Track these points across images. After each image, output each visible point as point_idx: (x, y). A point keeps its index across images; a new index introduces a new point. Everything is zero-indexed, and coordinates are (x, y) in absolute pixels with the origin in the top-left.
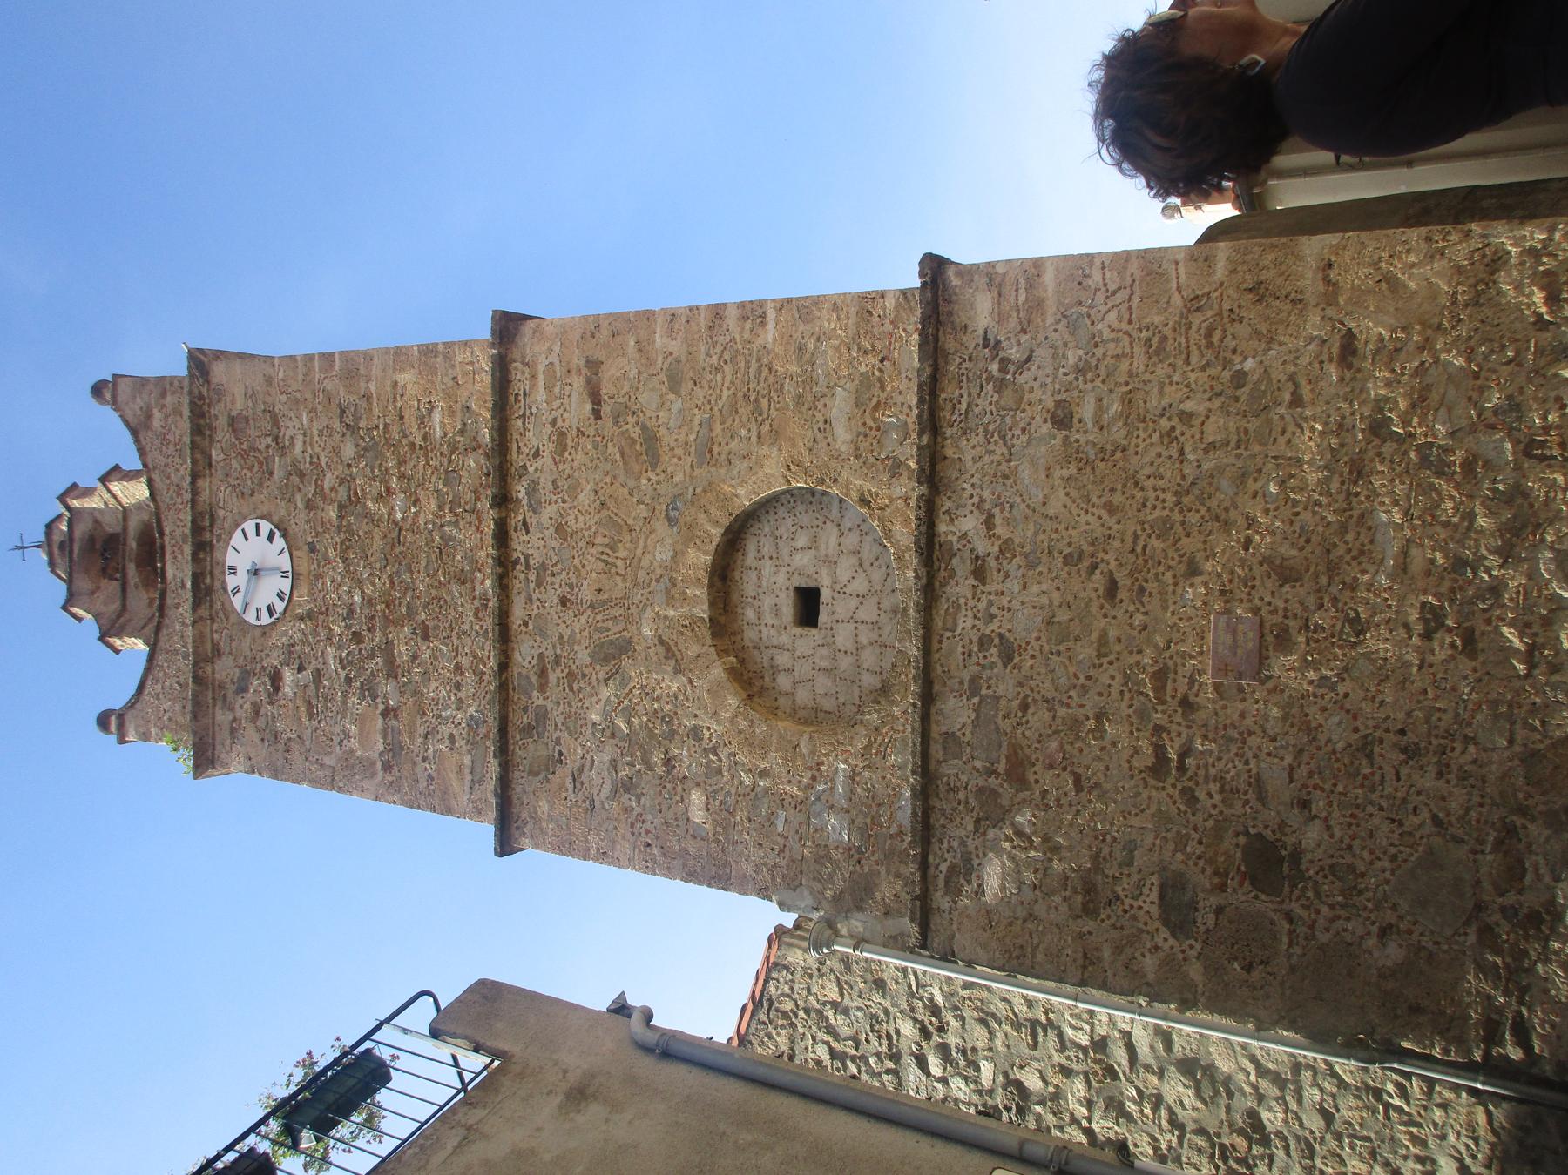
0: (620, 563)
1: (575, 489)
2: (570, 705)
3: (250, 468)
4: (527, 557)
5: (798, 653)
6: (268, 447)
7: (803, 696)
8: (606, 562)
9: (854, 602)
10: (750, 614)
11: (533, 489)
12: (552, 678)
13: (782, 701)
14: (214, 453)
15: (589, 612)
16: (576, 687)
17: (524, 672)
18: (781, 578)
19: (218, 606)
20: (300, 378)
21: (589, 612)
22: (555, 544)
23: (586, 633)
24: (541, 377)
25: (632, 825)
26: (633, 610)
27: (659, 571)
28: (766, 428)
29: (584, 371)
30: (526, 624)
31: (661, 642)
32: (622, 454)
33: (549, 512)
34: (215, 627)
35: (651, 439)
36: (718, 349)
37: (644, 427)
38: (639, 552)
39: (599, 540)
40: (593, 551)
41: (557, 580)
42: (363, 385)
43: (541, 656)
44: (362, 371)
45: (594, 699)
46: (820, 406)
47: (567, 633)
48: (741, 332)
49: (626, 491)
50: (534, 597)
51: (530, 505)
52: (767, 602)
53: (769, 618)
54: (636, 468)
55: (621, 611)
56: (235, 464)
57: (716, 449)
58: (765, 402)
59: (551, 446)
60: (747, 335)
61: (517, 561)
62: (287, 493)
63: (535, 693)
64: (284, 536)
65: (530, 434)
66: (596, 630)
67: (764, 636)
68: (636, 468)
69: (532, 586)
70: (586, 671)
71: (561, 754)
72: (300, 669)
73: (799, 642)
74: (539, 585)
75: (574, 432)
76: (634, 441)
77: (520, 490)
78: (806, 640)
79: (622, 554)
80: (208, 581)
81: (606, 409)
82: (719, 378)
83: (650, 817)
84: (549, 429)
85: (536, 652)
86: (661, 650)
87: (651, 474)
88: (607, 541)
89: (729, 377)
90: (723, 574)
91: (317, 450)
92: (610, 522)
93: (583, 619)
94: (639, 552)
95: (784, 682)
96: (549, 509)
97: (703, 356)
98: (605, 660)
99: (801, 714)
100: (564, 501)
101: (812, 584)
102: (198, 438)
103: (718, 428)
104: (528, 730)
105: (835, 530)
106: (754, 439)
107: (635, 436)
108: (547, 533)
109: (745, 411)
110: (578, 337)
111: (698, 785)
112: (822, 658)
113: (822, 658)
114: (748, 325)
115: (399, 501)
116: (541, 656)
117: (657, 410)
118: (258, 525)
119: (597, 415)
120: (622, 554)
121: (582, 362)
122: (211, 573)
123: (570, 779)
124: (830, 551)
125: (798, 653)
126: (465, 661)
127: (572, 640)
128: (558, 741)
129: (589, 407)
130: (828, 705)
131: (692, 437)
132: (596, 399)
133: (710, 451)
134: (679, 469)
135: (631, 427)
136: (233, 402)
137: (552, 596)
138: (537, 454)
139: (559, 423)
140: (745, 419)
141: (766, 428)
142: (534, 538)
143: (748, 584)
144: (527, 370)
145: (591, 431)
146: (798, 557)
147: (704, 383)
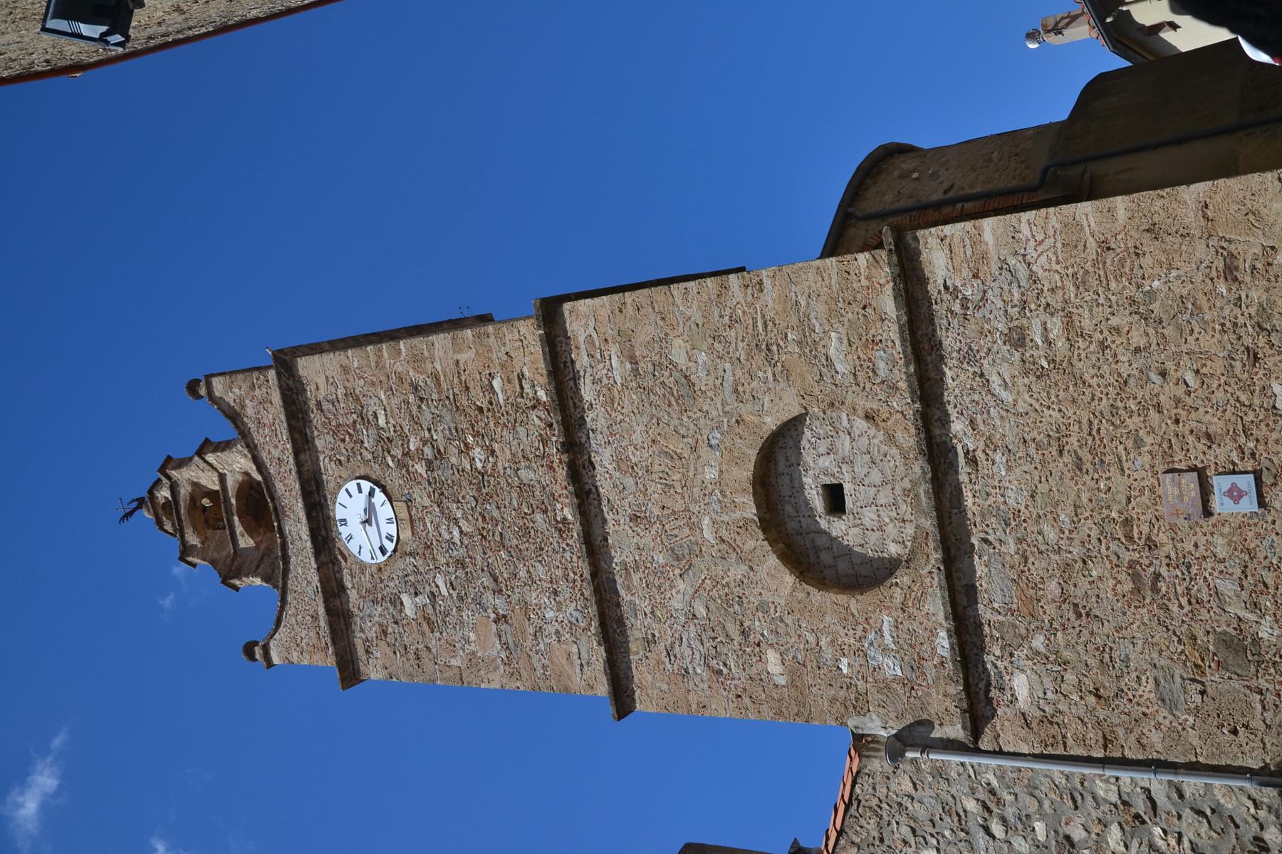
10: (789, 509)
64: (384, 490)
80: (324, 533)
114: (749, 291)
124: (847, 453)
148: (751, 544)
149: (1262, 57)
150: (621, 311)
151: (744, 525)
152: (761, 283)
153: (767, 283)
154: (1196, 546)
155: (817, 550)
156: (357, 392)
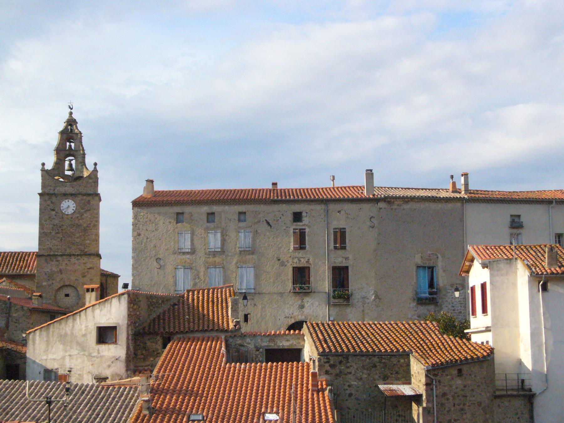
1: (79, 265)
11: (79, 259)
33: (76, 262)
35: (84, 277)
62: (79, 213)
77: (79, 257)
151: (64, 282)
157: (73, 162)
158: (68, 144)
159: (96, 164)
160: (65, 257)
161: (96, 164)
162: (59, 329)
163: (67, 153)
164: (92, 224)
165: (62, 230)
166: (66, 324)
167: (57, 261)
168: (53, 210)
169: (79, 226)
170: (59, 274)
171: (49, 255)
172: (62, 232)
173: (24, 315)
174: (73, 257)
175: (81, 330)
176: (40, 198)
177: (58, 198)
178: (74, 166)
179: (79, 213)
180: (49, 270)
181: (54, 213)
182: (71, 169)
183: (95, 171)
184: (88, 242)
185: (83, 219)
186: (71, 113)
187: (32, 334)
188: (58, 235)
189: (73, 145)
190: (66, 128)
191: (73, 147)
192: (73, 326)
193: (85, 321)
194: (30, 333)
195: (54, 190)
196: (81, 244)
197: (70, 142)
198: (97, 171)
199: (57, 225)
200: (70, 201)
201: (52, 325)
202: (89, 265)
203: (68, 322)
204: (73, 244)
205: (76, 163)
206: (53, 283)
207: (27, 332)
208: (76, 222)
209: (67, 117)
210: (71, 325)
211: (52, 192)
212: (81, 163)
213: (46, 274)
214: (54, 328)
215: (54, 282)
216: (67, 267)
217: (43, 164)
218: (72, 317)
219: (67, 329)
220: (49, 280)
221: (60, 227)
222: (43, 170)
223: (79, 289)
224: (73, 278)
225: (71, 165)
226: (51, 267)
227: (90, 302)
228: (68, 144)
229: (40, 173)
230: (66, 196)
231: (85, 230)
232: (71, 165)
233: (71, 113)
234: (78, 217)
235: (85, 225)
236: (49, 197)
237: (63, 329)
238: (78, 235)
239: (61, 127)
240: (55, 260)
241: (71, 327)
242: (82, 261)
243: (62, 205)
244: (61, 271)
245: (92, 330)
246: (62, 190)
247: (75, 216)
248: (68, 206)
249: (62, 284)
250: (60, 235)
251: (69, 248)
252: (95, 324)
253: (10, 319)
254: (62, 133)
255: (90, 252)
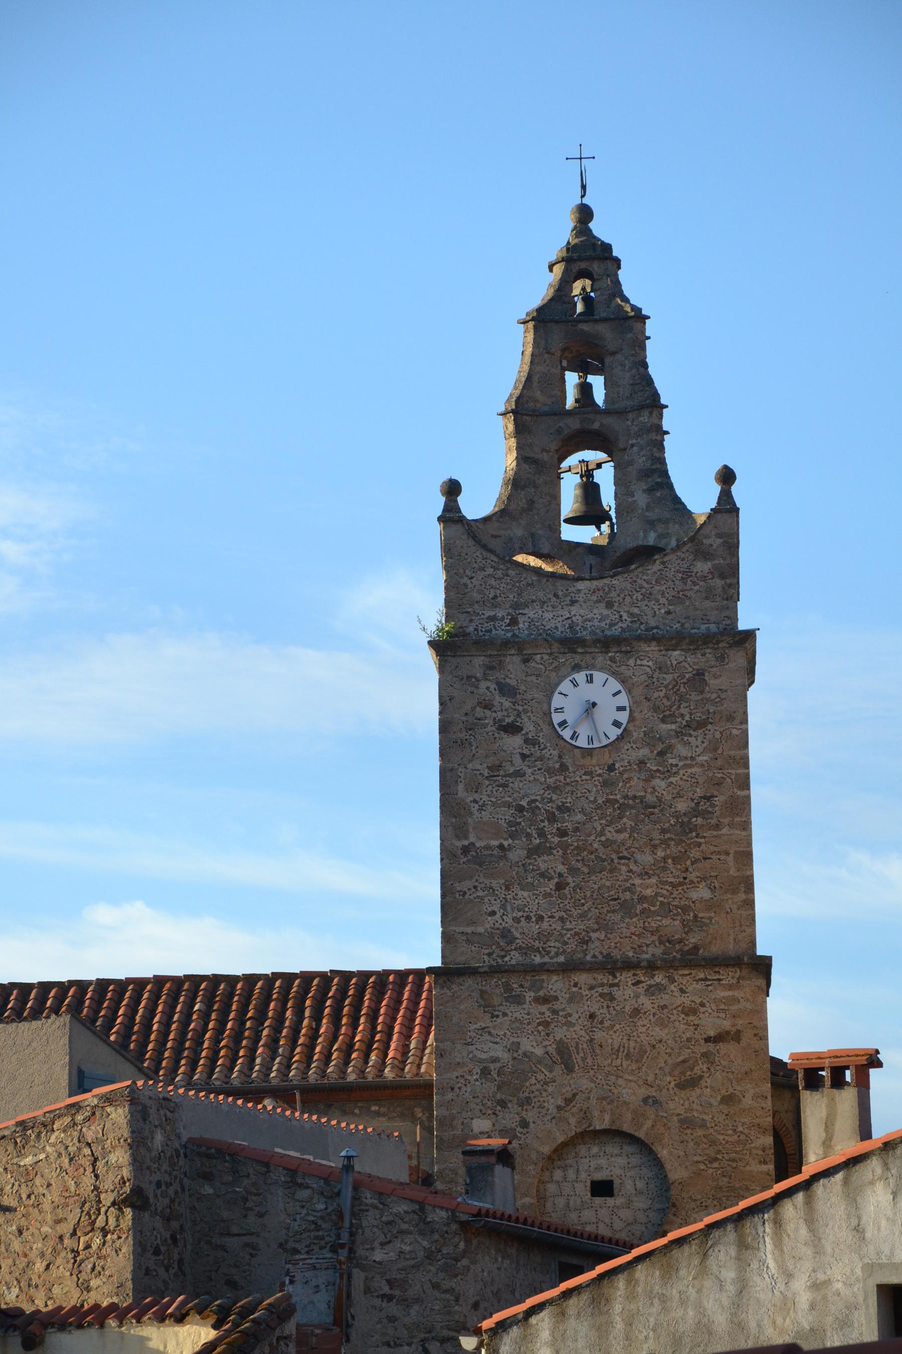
0: (619, 1061)
1: (662, 1024)
2: (529, 1024)
3: (667, 697)
4: (617, 985)
5: (576, 1185)
6: (682, 716)
7: (552, 1188)
8: (618, 1051)
9: (607, 1221)
10: (595, 1150)
11: (660, 988)
12: (543, 1008)
13: (547, 1173)
14: (677, 653)
15: (588, 1037)
16: (540, 1028)
17: (545, 985)
18: (618, 1171)
19: (744, 1300)
20: (732, 753)
21: (588, 1037)
22: (627, 1008)
23: (574, 1036)
24: (730, 993)
25: (462, 1076)
26: (592, 1072)
27: (616, 1091)
28: (702, 1167)
29: (734, 1029)
30: (575, 985)
31: (574, 1095)
32: (684, 1061)
33: (646, 1002)
34: (546, 657)
35: (693, 1083)
36: (746, 1131)
37: (701, 1077)
38: (627, 1076)
39: (632, 1044)
40: (625, 1041)
41: (605, 1011)
42: (726, 821)
43: (556, 998)
44: (737, 819)
45: (535, 1044)
46: (715, 1202)
47: (572, 1019)
48: (755, 1148)
49: (663, 1065)
50: (593, 992)
51: (650, 986)
52: (603, 1162)
53: (594, 1163)
54: (676, 1073)
55: (590, 1064)
56: (669, 677)
57: (689, 1131)
58: (716, 1165)
59: (688, 1003)
60: (754, 1151)
61: (615, 977)
62: (650, 738)
63: (533, 994)
64: (620, 738)
65: (695, 986)
66: (577, 1044)
67: (583, 1160)
68: (676, 1073)
69: (600, 989)
70: (551, 1037)
71: (497, 1016)
72: (524, 757)
73: (582, 1185)
74: (601, 995)
75: (696, 1022)
76: (692, 1070)
77: (659, 978)
78: (584, 1190)
79: (625, 1063)
80: (580, 650)
81: (711, 1046)
82: (730, 1132)
83: (469, 1090)
84: (698, 1001)
85: (558, 993)
86: (569, 1095)
87: (673, 1084)
88: (632, 1050)
89: (730, 1139)
90: (614, 1134)
91: (681, 772)
92: (642, 1052)
93: (583, 1033)
94: (627, 1076)
95: (558, 1174)
96: (649, 1002)
97: (742, 1120)
98: (559, 1051)
99: (541, 1187)
100: (654, 1014)
101: (616, 1191)
102: (687, 641)
103: (700, 1132)
104: (508, 987)
105: (645, 1206)
106: (696, 1158)
107: (695, 1071)
108: (634, 1001)
109: (711, 1152)
110: (755, 1024)
111: (494, 1125)
112: (575, 1201)
113: (575, 1201)
114: (760, 1152)
115: (646, 858)
116: (556, 998)
117: (711, 1087)
118: (619, 692)
119: (708, 1040)
120: (625, 1063)
121: (739, 1027)
122: (587, 652)
123: (484, 1026)
124: (635, 1204)
125: (576, 1185)
126: (545, 925)
127: (569, 1024)
128: (505, 1014)
129: (712, 1033)
130: (549, 1205)
131: (696, 1114)
132: (718, 1039)
133: (688, 1127)
134: (677, 1104)
135: (702, 1067)
136: (716, 677)
137: (595, 1008)
138: (682, 991)
139: (702, 1009)
140: (707, 1152)
141: (702, 1167)
142: (629, 991)
143: (612, 1148)
144: (735, 981)
145: (698, 1036)
146: (630, 1182)
147: (727, 1121)
148: (573, 1121)
149: (147, 1300)
150: (755, 1035)
151: (586, 1114)
152: (765, 1163)
153: (765, 1168)
154: (644, 1026)
155: (564, 1168)
156: (709, 727)
157: (605, 478)
158: (572, 379)
159: (727, 477)
160: (583, 978)
161: (727, 477)
162: (664, 1299)
163: (574, 424)
164: (720, 800)
165: (562, 833)
166: (703, 1270)
167: (546, 1000)
168: (512, 729)
169: (648, 808)
170: (559, 1070)
171: (496, 971)
172: (565, 847)
173: (430, 1256)
174: (625, 977)
175: (787, 1304)
176: (441, 669)
177: (540, 658)
178: (608, 498)
179: (650, 738)
180: (499, 1052)
181: (514, 742)
182: (591, 512)
183: (727, 507)
184: (702, 893)
185: (668, 773)
186: (585, 214)
187: (515, 1331)
188: (542, 863)
189: (597, 382)
190: (561, 292)
191: (599, 395)
192: (743, 1286)
193: (808, 1252)
194: (502, 1326)
195: (514, 622)
196: (667, 910)
197: (584, 369)
198: (734, 511)
199: (533, 808)
200: (599, 676)
201: (621, 1282)
202: (711, 1023)
203: (712, 1262)
204: (627, 908)
205: (619, 481)
206: (524, 1124)
207: (487, 1324)
208: (636, 786)
209: (561, 233)
210: (729, 1274)
211: (501, 632)
212: (645, 474)
213: (485, 1072)
214: (631, 1296)
215: (530, 1116)
216: (599, 1035)
217: (452, 489)
218: (727, 1240)
219: (710, 1304)
220: (503, 1104)
221: (552, 818)
222: (451, 516)
223: (663, 1153)
224: (631, 1092)
225: (590, 490)
226: (509, 1034)
227: (827, 1144)
228: (572, 379)
229: (435, 531)
230: (578, 649)
231: (685, 826)
232: (590, 490)
233: (585, 214)
234: (642, 763)
235: (682, 806)
236: (483, 654)
237: (683, 1302)
238: (646, 858)
239: (538, 287)
240: (529, 995)
241: (731, 1289)
242: (673, 998)
243: (557, 701)
244: (564, 1057)
245: (851, 1307)
246: (553, 619)
247: (633, 753)
248: (591, 704)
249: (573, 1125)
250: (553, 864)
251: (603, 925)
252: (870, 1268)
253: (359, 1277)
254: (546, 319)
255: (716, 949)
